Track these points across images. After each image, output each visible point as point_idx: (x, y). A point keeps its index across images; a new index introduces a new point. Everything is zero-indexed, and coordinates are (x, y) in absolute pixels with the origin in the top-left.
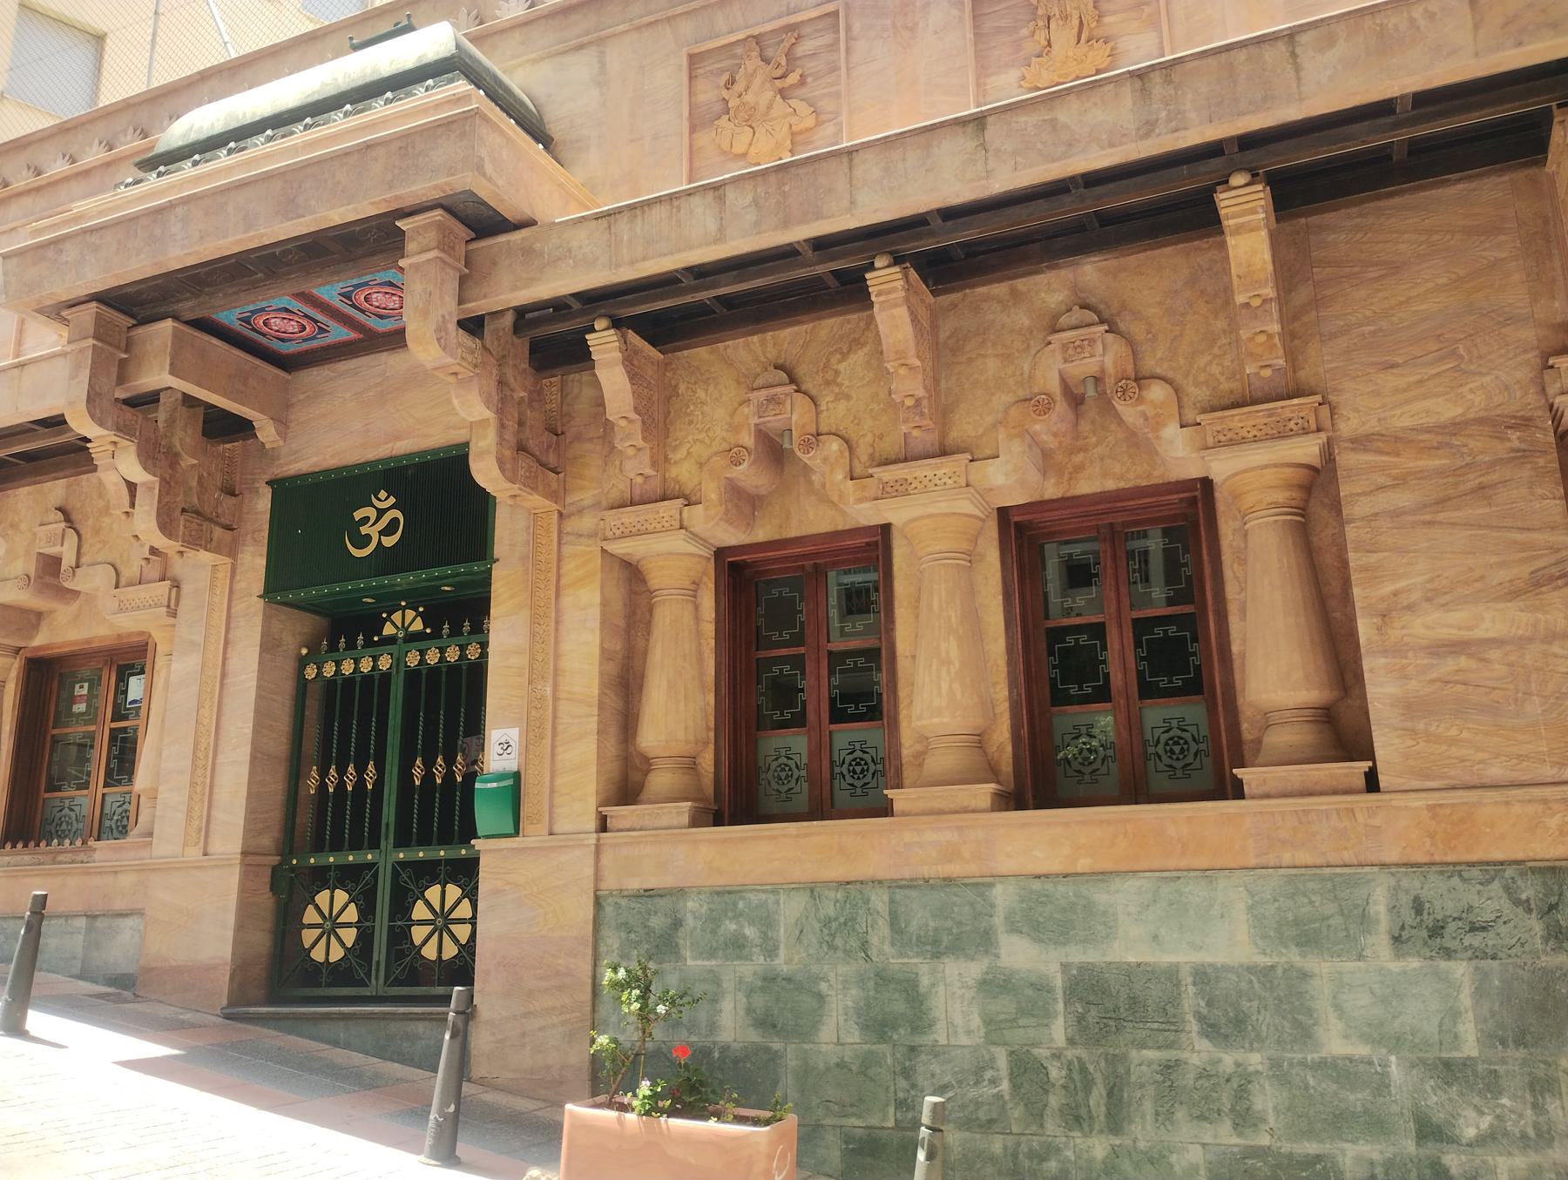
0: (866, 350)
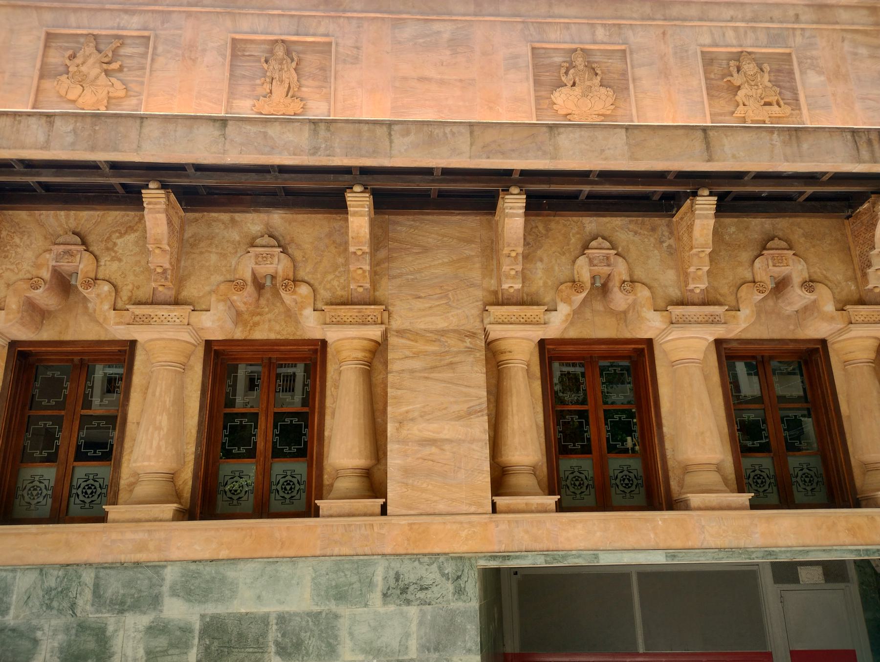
0: (137, 234)
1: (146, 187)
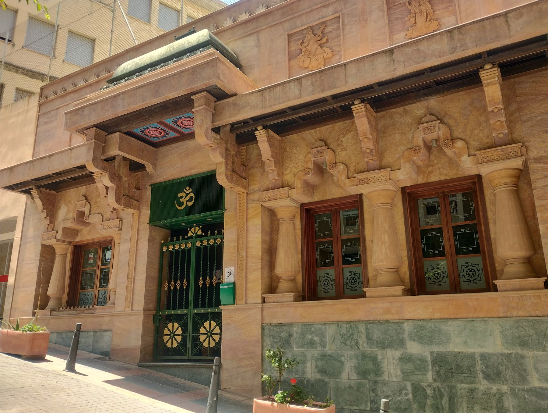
0: (352, 133)
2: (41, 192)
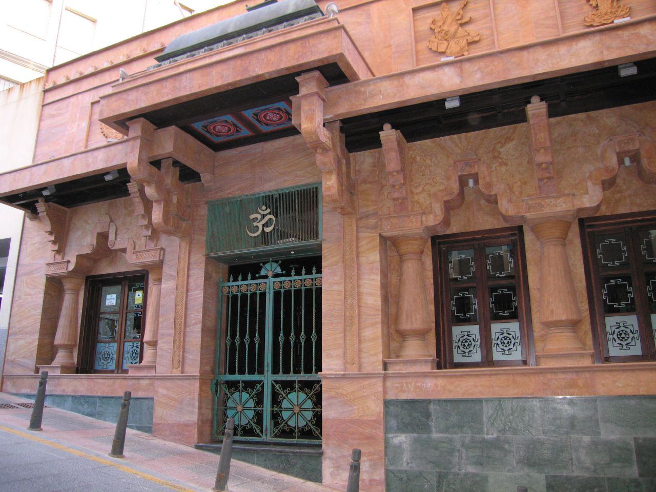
0: (514, 142)
1: (37, 202)
2: (49, 207)
